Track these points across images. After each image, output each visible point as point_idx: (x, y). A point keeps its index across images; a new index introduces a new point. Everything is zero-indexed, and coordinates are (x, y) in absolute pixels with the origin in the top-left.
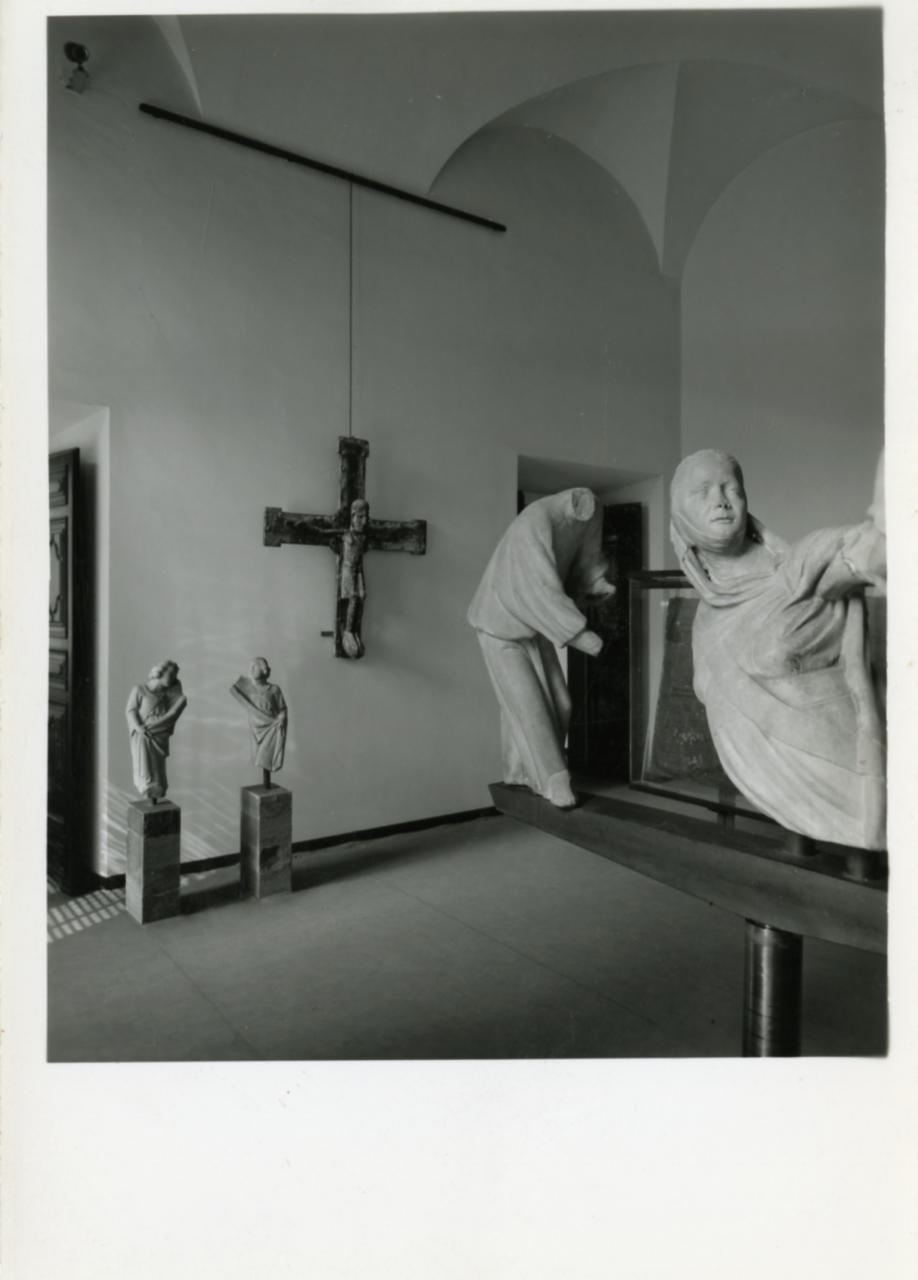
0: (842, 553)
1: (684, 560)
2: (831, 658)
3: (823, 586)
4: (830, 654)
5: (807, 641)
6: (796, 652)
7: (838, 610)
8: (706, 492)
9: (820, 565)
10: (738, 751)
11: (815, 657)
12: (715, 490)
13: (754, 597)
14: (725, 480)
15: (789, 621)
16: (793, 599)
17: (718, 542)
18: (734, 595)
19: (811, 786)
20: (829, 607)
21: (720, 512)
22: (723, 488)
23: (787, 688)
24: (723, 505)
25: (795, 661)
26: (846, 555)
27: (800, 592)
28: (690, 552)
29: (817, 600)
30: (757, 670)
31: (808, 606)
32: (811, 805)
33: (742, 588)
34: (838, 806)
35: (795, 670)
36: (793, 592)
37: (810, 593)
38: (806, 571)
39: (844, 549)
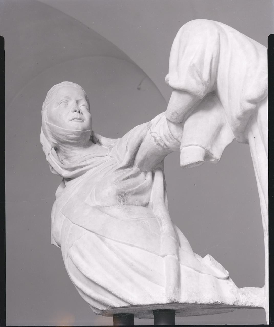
0: (151, 130)
1: (49, 154)
2: (144, 202)
3: (139, 157)
4: (144, 198)
5: (128, 188)
6: (123, 191)
7: (149, 176)
8: (66, 102)
9: (137, 141)
10: (83, 256)
11: (134, 197)
12: (72, 103)
13: (96, 166)
14: (79, 98)
15: (118, 176)
16: (121, 165)
17: (73, 133)
18: (81, 167)
19: (131, 266)
20: (142, 175)
21: (76, 115)
22: (77, 102)
23: (117, 211)
24: (78, 111)
25: (122, 196)
26: (152, 131)
27: (124, 163)
28: (53, 150)
29: (135, 169)
30: (97, 203)
31: (130, 171)
32: (131, 280)
33: (88, 162)
34: (149, 278)
35: (122, 203)
36: (121, 162)
37: (130, 164)
38: (129, 149)
39: (151, 128)
